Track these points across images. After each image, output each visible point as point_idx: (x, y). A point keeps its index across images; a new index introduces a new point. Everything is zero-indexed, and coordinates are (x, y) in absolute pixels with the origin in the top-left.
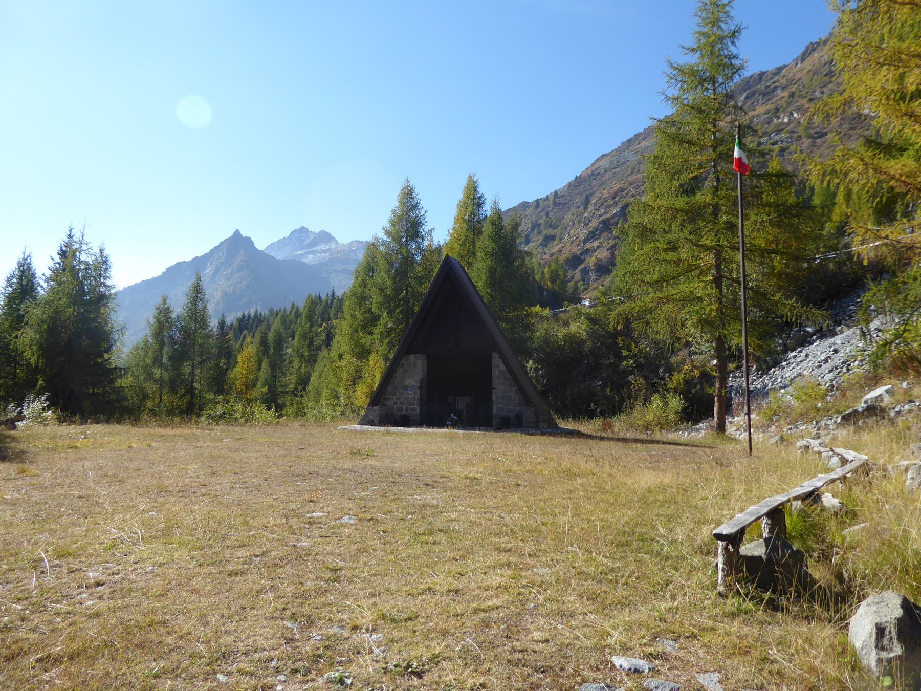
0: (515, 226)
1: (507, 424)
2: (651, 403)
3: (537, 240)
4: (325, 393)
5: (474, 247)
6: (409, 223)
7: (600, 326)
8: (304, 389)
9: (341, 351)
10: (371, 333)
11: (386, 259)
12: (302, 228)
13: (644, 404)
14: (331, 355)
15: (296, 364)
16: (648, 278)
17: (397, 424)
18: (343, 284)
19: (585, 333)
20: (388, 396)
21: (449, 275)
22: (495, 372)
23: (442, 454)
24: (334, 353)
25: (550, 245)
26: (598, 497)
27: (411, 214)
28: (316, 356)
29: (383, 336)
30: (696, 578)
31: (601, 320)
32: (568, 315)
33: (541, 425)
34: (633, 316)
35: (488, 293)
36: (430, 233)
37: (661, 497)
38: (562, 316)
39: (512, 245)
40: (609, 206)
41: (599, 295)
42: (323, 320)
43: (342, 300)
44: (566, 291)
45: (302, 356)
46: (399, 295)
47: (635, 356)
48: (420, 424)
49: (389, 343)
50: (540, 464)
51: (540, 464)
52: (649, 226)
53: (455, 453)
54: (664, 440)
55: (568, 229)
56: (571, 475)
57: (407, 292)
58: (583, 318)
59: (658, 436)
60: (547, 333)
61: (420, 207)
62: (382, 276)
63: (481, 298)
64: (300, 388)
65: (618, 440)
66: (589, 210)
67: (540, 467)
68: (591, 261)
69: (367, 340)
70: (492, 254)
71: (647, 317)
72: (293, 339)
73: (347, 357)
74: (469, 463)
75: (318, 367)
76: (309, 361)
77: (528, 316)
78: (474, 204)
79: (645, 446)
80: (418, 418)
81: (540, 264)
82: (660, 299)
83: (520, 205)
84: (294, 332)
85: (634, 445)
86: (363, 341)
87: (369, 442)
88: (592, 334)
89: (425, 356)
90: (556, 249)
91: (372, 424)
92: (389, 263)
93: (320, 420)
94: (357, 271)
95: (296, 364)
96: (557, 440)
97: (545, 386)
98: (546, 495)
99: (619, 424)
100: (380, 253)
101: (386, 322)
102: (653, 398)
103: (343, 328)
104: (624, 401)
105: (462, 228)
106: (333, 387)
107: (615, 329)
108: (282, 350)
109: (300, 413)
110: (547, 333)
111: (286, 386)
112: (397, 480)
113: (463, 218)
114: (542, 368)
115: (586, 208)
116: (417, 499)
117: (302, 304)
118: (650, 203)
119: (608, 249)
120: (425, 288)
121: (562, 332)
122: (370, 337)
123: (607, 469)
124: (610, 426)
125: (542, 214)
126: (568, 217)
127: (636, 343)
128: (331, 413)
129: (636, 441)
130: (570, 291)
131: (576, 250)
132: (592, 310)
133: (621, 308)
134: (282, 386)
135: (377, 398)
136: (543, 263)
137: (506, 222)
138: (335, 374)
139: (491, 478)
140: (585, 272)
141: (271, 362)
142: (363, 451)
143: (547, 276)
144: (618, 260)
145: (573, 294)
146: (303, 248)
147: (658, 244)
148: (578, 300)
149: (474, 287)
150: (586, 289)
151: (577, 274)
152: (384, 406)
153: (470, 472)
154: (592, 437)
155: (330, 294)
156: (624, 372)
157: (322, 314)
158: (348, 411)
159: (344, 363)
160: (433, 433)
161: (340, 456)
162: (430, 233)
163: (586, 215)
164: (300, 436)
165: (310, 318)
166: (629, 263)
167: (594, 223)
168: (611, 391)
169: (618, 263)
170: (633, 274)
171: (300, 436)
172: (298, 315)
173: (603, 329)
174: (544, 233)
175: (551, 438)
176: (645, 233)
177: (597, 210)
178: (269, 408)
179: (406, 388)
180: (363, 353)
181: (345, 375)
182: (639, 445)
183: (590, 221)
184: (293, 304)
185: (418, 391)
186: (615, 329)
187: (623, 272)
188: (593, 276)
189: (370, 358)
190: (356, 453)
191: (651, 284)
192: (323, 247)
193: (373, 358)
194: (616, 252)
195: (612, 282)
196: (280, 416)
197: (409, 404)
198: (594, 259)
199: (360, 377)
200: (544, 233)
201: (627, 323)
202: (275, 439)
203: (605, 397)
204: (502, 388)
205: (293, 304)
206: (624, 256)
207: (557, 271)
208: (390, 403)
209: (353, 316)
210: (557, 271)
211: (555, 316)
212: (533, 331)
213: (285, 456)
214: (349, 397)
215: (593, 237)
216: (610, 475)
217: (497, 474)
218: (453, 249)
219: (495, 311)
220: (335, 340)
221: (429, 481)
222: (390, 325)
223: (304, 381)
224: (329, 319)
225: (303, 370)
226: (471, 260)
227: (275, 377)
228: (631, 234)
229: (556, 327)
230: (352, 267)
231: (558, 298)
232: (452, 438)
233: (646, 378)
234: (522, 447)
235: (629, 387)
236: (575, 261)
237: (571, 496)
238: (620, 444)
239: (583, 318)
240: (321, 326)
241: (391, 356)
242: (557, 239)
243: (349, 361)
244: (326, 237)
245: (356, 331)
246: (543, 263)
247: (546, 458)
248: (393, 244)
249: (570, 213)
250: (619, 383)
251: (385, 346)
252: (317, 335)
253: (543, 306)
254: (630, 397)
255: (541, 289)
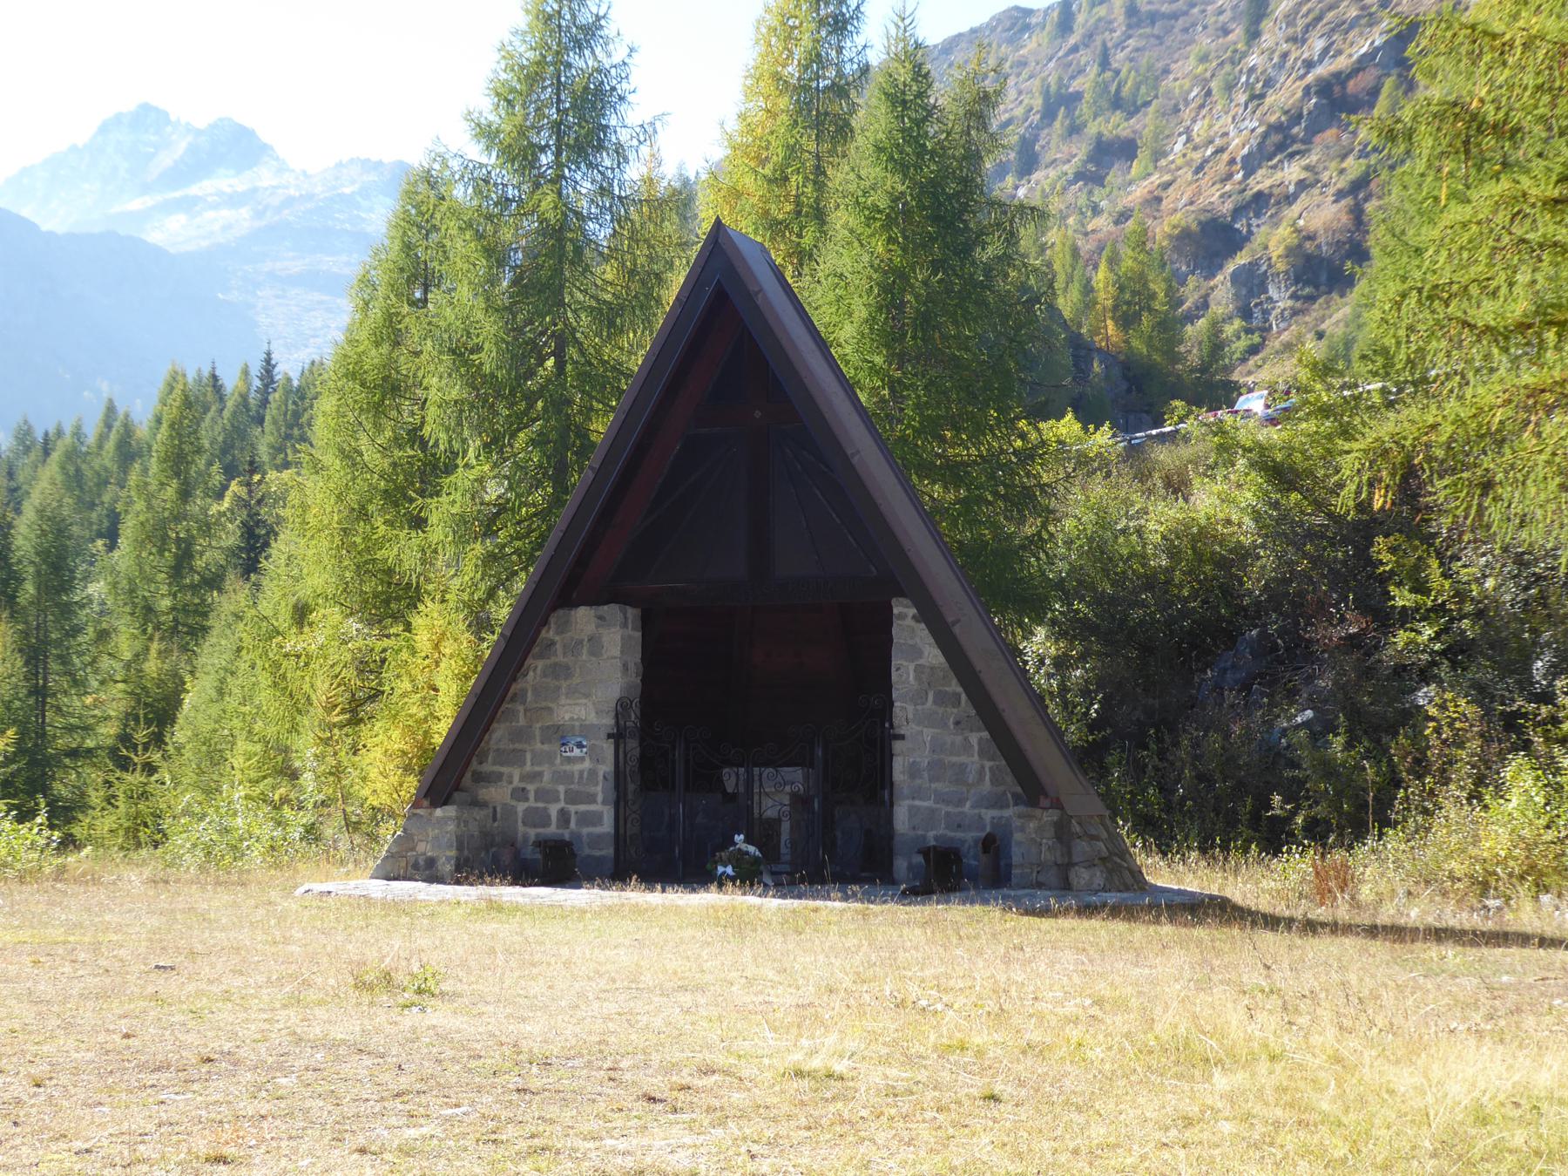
0: (981, 106)
1: (947, 873)
2: (1500, 791)
3: (1064, 156)
4: (244, 754)
5: (820, 186)
6: (564, 103)
7: (1307, 493)
8: (158, 740)
9: (304, 592)
10: (419, 523)
11: (480, 236)
12: (146, 108)
13: (1474, 796)
14: (265, 607)
15: (125, 643)
16: (1486, 313)
17: (524, 874)
18: (308, 327)
19: (1248, 523)
20: (488, 767)
21: (727, 324)
22: (904, 675)
23: (701, 988)
24: (274, 600)
25: (1114, 177)
26: (1288, 1139)
27: (573, 58)
28: (203, 611)
29: (464, 529)
30: (1340, 1144)
31: (1310, 473)
32: (1185, 452)
33: (1081, 876)
34: (1429, 459)
35: (874, 370)
36: (647, 132)
37: (1518, 1138)
38: (1164, 456)
39: (966, 182)
40: (1343, 27)
41: (1304, 375)
42: (230, 472)
43: (301, 394)
44: (1175, 358)
45: (149, 610)
46: (531, 374)
47: (1440, 609)
48: (617, 872)
49: (490, 559)
50: (1076, 1021)
51: (1076, 1021)
52: (1491, 115)
53: (750, 981)
54: (1549, 931)
55: (1187, 114)
56: (1190, 1059)
57: (560, 365)
58: (1241, 463)
59: (1526, 915)
60: (1103, 523)
61: (609, 30)
62: (462, 301)
63: (849, 387)
64: (141, 736)
65: (1373, 931)
66: (1267, 40)
67: (1075, 1033)
68: (1272, 241)
69: (403, 551)
70: (893, 219)
71: (1487, 462)
72: (112, 546)
73: (329, 617)
74: (807, 1017)
75: (213, 654)
76: (174, 630)
77: (1028, 456)
78: (821, 23)
79: (1473, 953)
80: (608, 851)
81: (1075, 252)
82: (1535, 392)
83: (997, 20)
84: (115, 519)
85: (1433, 951)
86: (388, 554)
87: (423, 942)
88: (1278, 527)
89: (632, 613)
90: (1139, 192)
91: (431, 874)
92: (489, 252)
93: (223, 856)
94: (366, 282)
95: (125, 643)
96: (1139, 932)
97: (1093, 726)
98: (1098, 1132)
99: (1380, 873)
100: (455, 212)
101: (479, 479)
102: (1508, 773)
103: (312, 503)
104: (1397, 783)
105: (771, 114)
106: (271, 731)
107: (1363, 507)
108: (66, 586)
109: (145, 832)
110: (1103, 523)
111: (87, 729)
112: (535, 1084)
113: (777, 77)
114: (1083, 658)
115: (1254, 35)
116: (614, 1152)
117: (144, 411)
118: (1498, 27)
119: (1340, 195)
120: (634, 350)
121: (1161, 518)
122: (417, 538)
123: (1326, 1037)
124: (1346, 880)
125: (1084, 56)
126: (1185, 71)
127: (1447, 561)
128: (267, 831)
129: (1440, 935)
130: (1194, 359)
131: (1215, 198)
132: (1274, 435)
133: (1384, 428)
134: (70, 729)
135: (449, 775)
136: (1086, 246)
137: (943, 94)
138: (279, 682)
139: (893, 1072)
140: (1252, 283)
141: (25, 634)
142: (400, 977)
143: (1105, 297)
144: (1377, 239)
145: (1204, 369)
146: (146, 189)
147: (1526, 182)
148: (1216, 391)
149: (823, 345)
150: (1254, 350)
151: (1222, 290)
152: (476, 803)
153: (813, 1052)
154: (1271, 922)
155: (256, 369)
156: (1400, 670)
157: (226, 449)
158: (330, 827)
159: (312, 640)
160: (667, 910)
161: (312, 995)
162: (647, 132)
163: (1253, 60)
164: (154, 922)
165: (178, 462)
166: (1418, 252)
167: (1287, 94)
168: (1349, 746)
169: (1375, 252)
170: (1433, 295)
171: (154, 922)
172: (128, 452)
173: (1319, 505)
174: (1092, 129)
175: (1119, 926)
176: (1477, 137)
177: (1298, 40)
178: (24, 816)
179: (560, 734)
180: (391, 600)
181: (321, 688)
182: (1451, 953)
183: (1269, 83)
184: (111, 410)
185: (608, 748)
186: (1363, 507)
187: (1394, 288)
188: (1280, 297)
189: (417, 621)
190: (377, 984)
191: (1499, 335)
192: (224, 182)
193: (428, 621)
194: (1370, 207)
195: (1356, 321)
196: (69, 843)
197: (573, 798)
198: (1284, 231)
199: (376, 695)
200: (1092, 129)
201: (1409, 484)
202: (58, 934)
203: (1328, 770)
204: (928, 733)
205: (111, 410)
206: (1400, 223)
207: (1142, 278)
208: (497, 794)
209: (350, 457)
210: (1142, 278)
211: (1133, 453)
212: (1049, 515)
213: (103, 995)
214: (337, 772)
215: (1280, 148)
216: (1337, 1059)
217: (910, 1060)
218: (736, 194)
219: (903, 439)
220: (280, 549)
221: (656, 1084)
222: (494, 491)
223: (158, 710)
224: (254, 467)
225: (152, 666)
226: (807, 241)
227: (40, 693)
228: (1426, 143)
229: (1139, 502)
230: (349, 263)
231: (1144, 390)
232: (739, 925)
233: (1482, 694)
234: (1006, 959)
235: (1417, 736)
236: (1214, 240)
237: (1188, 1135)
238: (1380, 949)
239: (1241, 463)
240: (220, 496)
241: (502, 611)
242: (1143, 155)
243: (336, 634)
244: (236, 145)
245: (362, 514)
246: (1086, 246)
247: (1099, 1002)
248: (507, 178)
249: (1194, 51)
250: (1379, 711)
251: (469, 570)
252: (207, 528)
253: (1089, 417)
254: (1420, 767)
255: (1081, 350)
